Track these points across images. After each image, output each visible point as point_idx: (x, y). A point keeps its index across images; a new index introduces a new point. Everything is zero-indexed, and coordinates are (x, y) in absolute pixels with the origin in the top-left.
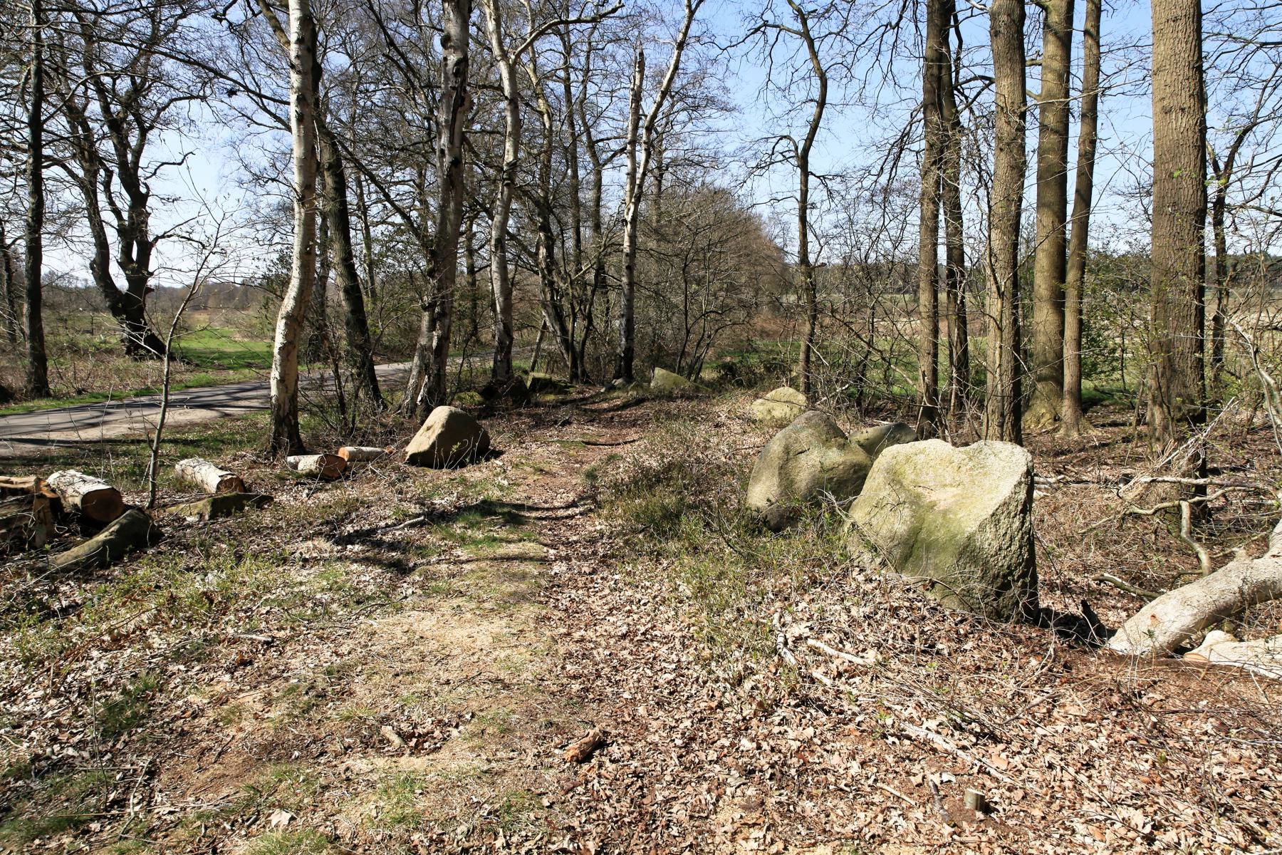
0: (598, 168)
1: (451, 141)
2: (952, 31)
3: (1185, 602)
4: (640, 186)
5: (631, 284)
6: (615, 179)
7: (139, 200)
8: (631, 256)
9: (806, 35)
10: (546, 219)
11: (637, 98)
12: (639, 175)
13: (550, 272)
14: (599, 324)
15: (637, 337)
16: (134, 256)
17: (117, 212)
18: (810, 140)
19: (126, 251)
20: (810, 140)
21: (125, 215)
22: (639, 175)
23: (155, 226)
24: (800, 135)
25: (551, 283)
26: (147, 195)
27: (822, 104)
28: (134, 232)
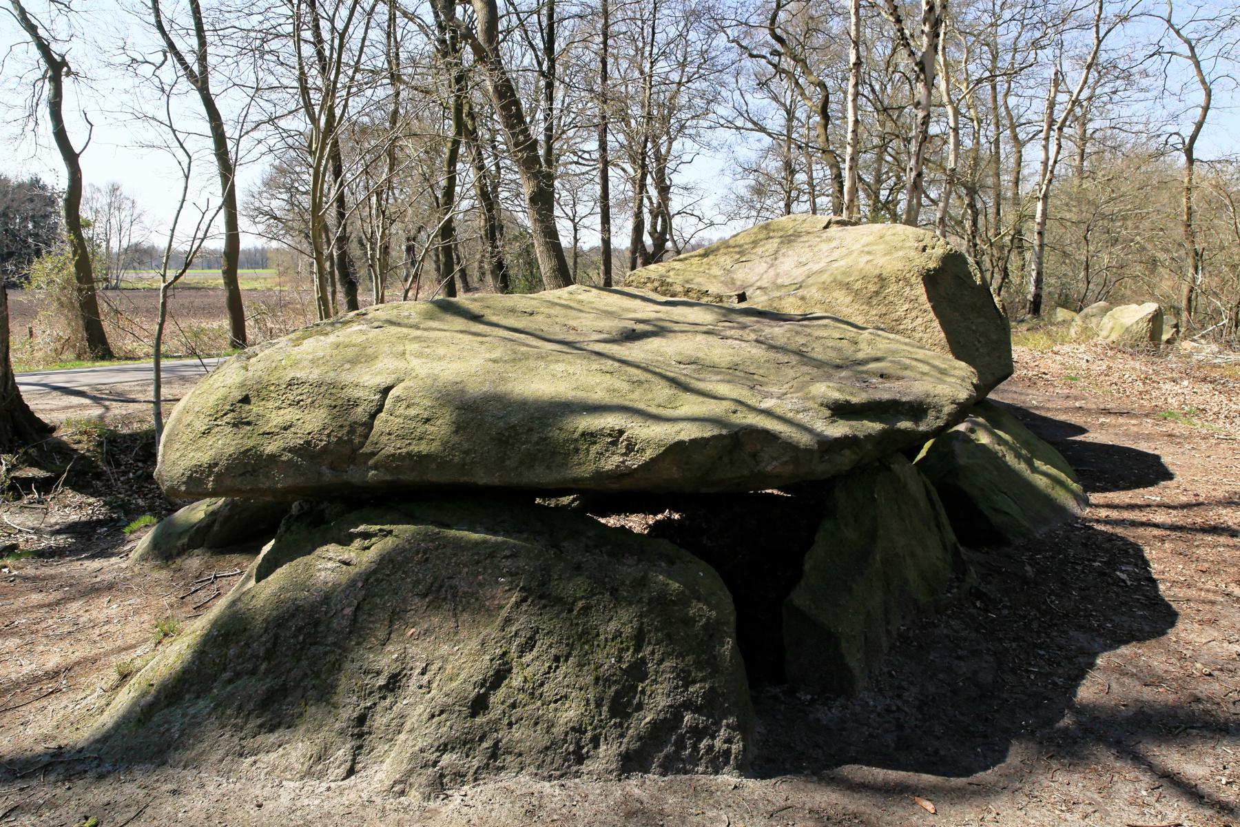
0: (1019, 144)
1: (917, 162)
2: (1096, 526)
3: (851, 427)
4: (1052, 172)
5: (1041, 246)
6: (1034, 154)
7: (664, 190)
8: (1043, 224)
9: (1193, 56)
10: (973, 199)
11: (1052, 105)
12: (1051, 162)
13: (974, 237)
14: (1014, 278)
15: (1046, 290)
16: (659, 229)
17: (651, 203)
18: (1193, 138)
19: (654, 226)
20: (1193, 138)
21: (655, 201)
22: (1051, 162)
23: (674, 205)
24: (1187, 132)
25: (975, 245)
26: (669, 187)
27: (1206, 109)
28: (662, 212)
